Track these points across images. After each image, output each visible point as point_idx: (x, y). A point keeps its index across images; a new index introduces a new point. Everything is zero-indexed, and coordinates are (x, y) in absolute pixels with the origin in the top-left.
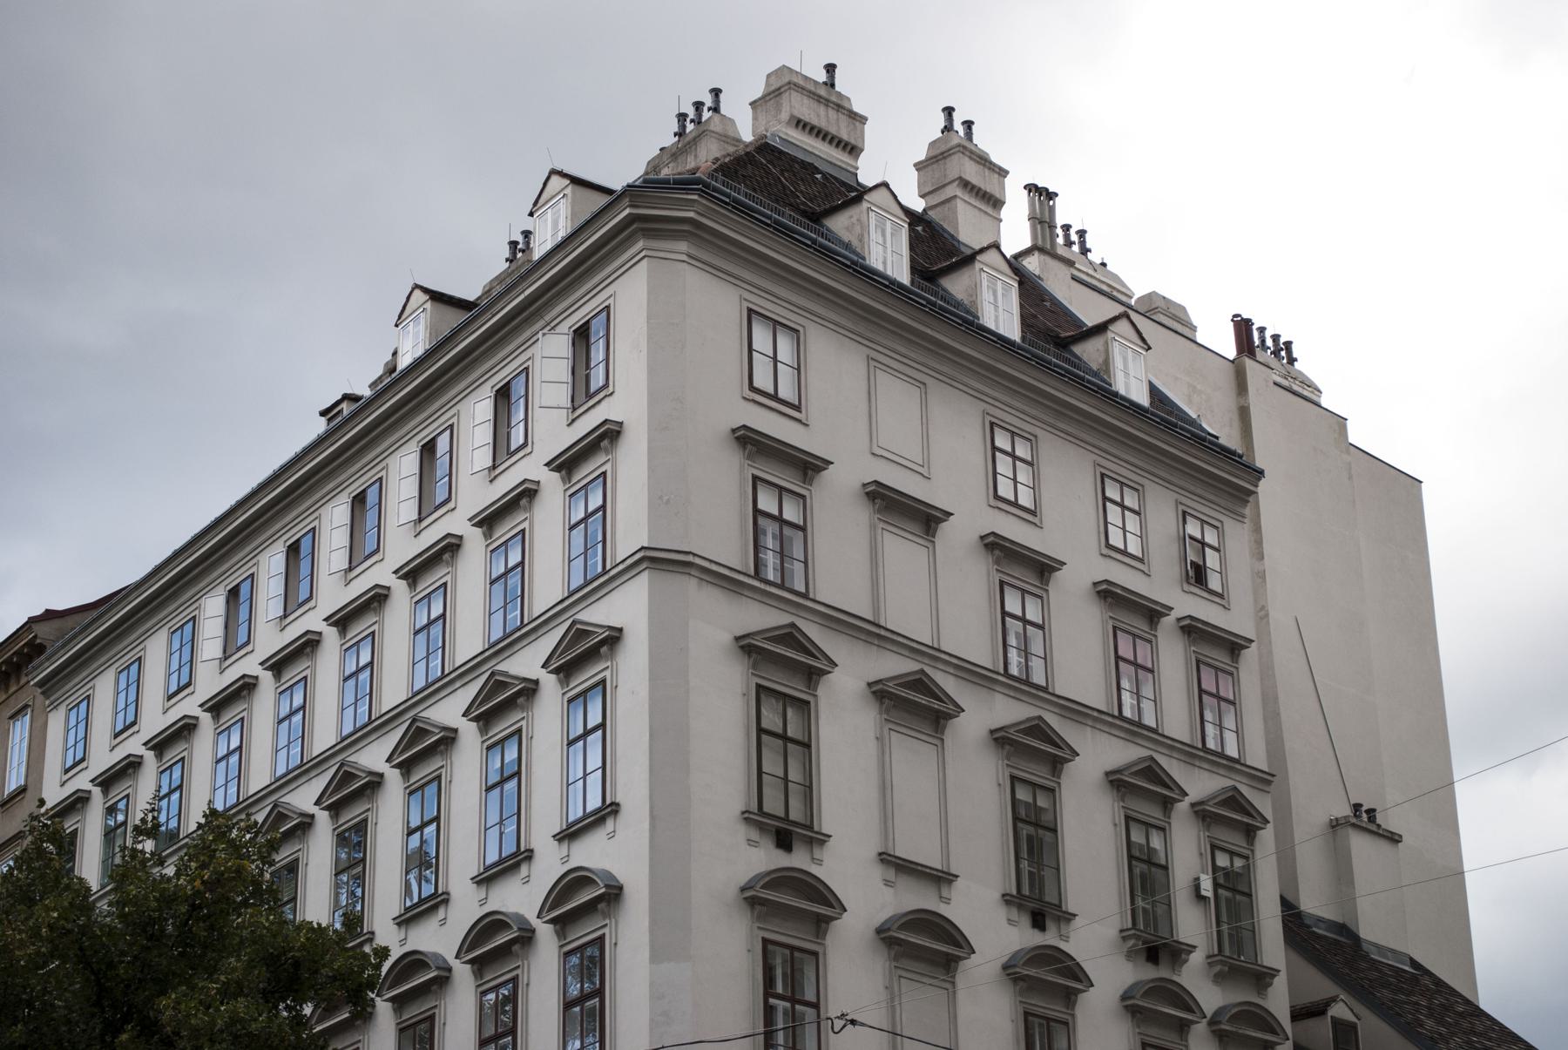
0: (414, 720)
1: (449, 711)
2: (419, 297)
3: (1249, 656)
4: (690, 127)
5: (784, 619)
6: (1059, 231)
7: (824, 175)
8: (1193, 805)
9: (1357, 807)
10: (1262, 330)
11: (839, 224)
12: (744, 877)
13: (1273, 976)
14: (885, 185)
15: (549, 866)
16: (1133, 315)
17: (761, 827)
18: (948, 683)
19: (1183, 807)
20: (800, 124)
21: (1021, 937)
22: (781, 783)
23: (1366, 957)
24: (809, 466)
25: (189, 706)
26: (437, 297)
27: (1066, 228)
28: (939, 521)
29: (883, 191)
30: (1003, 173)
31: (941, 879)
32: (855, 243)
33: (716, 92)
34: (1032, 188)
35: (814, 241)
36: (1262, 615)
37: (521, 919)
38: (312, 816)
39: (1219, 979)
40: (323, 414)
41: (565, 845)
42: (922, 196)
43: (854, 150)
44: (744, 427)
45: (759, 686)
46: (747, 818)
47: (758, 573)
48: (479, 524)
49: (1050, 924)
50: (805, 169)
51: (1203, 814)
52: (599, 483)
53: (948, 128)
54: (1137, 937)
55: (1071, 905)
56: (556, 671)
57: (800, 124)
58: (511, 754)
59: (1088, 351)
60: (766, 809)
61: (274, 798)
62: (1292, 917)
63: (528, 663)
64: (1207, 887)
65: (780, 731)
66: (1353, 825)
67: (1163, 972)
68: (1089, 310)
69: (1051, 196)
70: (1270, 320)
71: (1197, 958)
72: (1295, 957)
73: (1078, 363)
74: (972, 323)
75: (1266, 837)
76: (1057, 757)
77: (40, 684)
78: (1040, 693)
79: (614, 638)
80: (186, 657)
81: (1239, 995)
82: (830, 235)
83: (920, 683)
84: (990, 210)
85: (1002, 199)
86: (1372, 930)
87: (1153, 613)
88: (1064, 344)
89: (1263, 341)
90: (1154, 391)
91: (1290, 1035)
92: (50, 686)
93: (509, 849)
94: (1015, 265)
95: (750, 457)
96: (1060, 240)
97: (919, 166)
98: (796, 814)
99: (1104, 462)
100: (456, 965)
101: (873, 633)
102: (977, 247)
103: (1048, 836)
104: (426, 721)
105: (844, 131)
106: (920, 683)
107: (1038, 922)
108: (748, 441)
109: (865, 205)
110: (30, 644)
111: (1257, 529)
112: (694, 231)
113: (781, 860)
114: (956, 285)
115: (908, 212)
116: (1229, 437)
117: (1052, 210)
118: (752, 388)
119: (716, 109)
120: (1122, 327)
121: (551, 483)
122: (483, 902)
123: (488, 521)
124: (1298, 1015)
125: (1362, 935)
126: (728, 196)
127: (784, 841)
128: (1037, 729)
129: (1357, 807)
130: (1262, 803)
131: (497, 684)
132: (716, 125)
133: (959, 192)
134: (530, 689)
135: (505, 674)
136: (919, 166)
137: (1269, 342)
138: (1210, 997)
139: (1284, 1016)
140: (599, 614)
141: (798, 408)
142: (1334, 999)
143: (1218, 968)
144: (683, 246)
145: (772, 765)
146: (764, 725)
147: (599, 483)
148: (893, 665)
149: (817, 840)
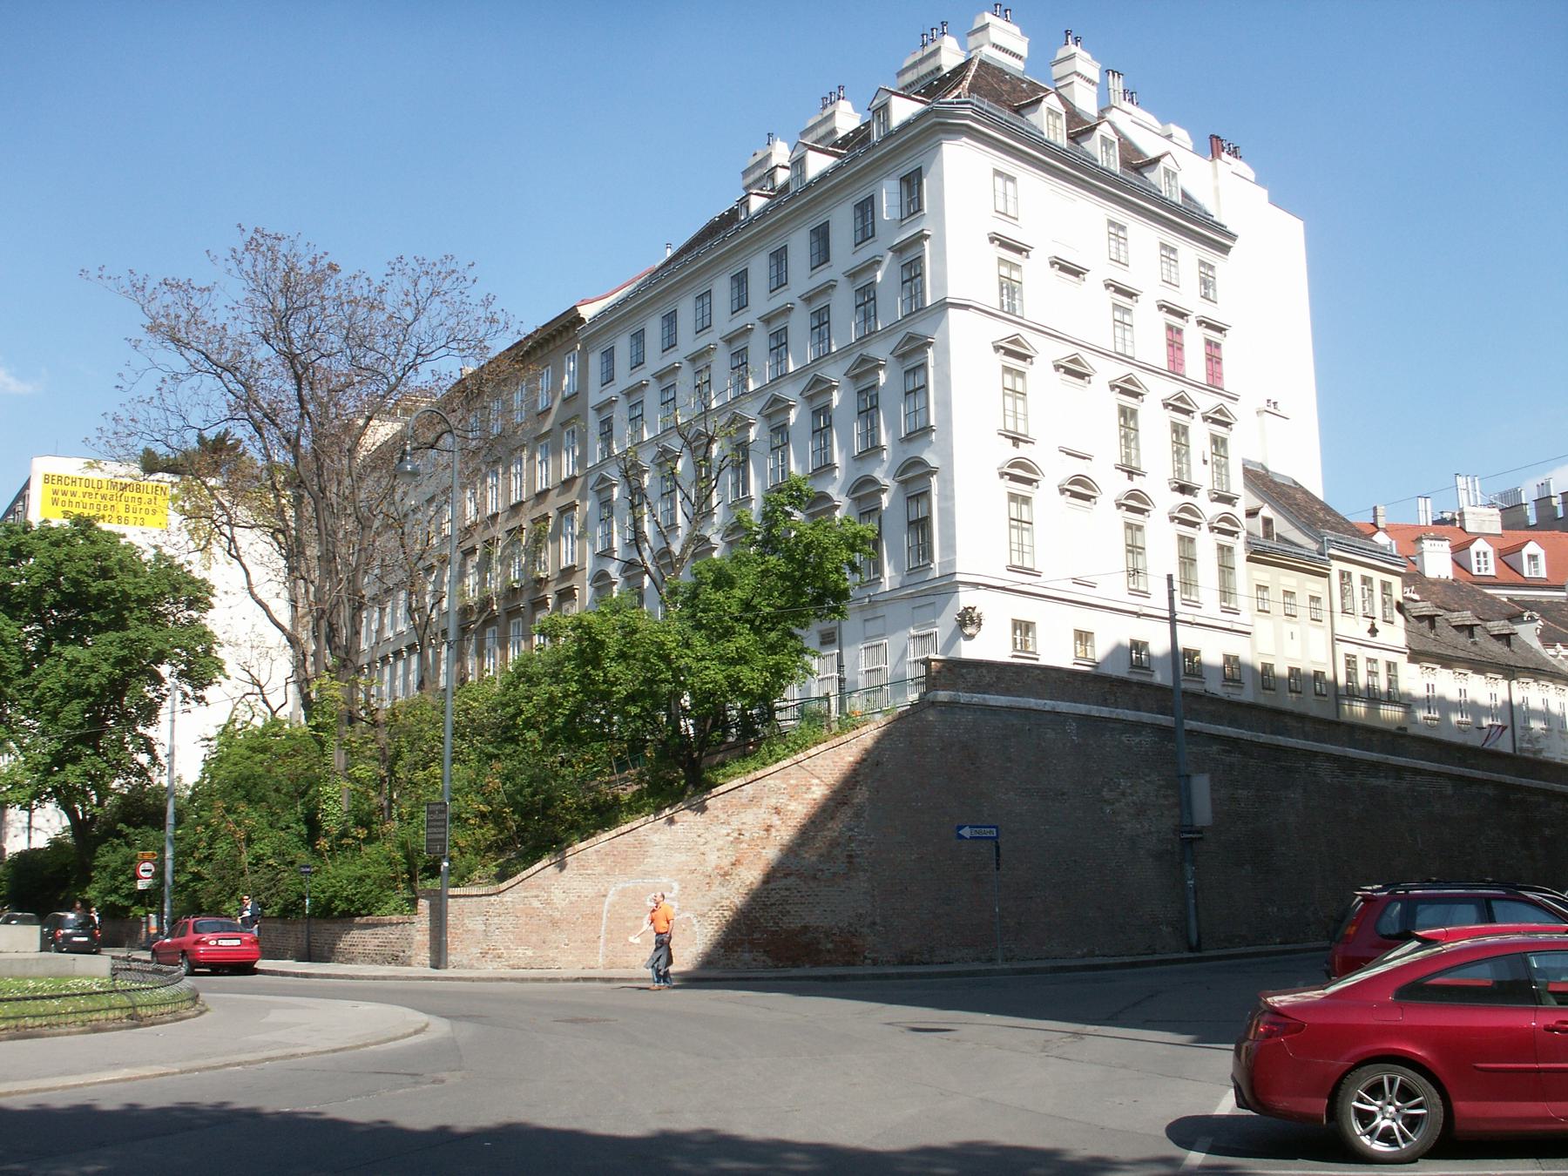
19: (1198, 415)
20: (995, 46)
21: (1123, 484)
41: (906, 443)
57: (995, 46)
67: (1187, 498)
99: (1111, 214)
127: (1016, 441)
148: (1064, 351)
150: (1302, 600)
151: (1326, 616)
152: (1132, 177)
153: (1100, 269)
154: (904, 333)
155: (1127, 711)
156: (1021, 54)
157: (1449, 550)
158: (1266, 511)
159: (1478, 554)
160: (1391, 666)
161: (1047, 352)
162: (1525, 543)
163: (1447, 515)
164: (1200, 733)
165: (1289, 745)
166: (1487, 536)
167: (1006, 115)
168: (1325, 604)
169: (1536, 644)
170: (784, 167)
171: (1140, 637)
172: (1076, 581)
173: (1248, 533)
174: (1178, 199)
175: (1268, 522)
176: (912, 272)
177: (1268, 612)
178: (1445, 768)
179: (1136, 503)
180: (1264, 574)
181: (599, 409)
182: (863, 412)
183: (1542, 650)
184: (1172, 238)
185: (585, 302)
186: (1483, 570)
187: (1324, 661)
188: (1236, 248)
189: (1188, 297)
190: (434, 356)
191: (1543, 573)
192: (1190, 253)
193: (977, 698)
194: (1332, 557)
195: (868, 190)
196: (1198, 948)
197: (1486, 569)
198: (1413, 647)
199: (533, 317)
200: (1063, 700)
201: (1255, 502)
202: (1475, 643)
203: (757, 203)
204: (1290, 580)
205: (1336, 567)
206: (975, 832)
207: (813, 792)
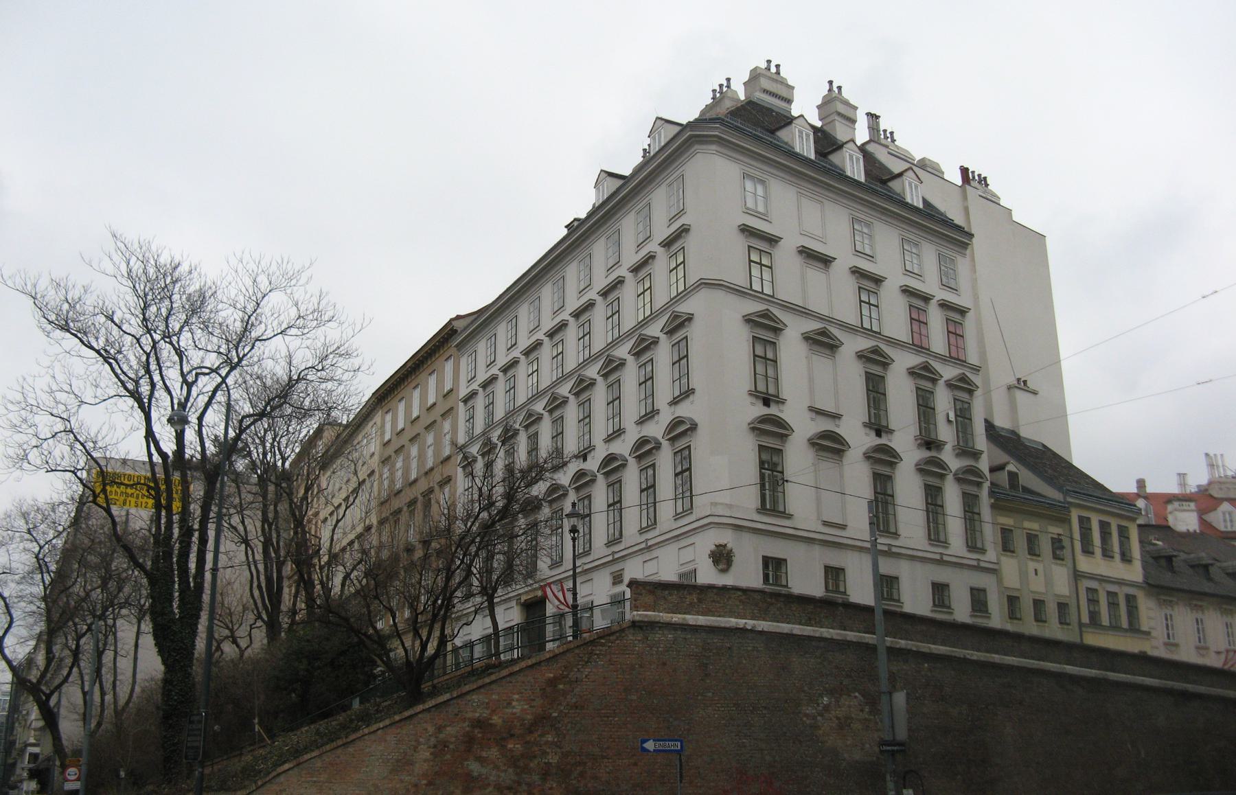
0: (608, 356)
1: (622, 352)
2: (603, 175)
3: (970, 315)
4: (718, 95)
6: (882, 133)
7: (776, 113)
8: (945, 381)
9: (1019, 380)
10: (973, 172)
11: (783, 134)
12: (749, 420)
13: (981, 454)
14: (802, 116)
15: (665, 417)
16: (914, 168)
17: (757, 397)
18: (835, 331)
19: (941, 382)
20: (765, 91)
21: (871, 440)
22: (869, 319)
24: (773, 240)
25: (516, 353)
26: (611, 175)
27: (885, 131)
28: (831, 262)
29: (802, 118)
30: (855, 108)
31: (836, 417)
32: (790, 143)
33: (728, 80)
34: (869, 114)
35: (771, 142)
36: (976, 298)
37: (656, 439)
38: (568, 398)
39: (958, 455)
40: (566, 227)
41: (673, 406)
43: (789, 101)
44: (744, 224)
45: (754, 337)
46: (751, 394)
47: (751, 289)
48: (632, 272)
49: (883, 434)
50: (766, 111)
51: (949, 385)
52: (808, 150)
53: (830, 90)
54: (922, 439)
55: (891, 426)
56: (666, 333)
57: (765, 91)
58: (649, 368)
59: (894, 185)
60: (758, 389)
61: (552, 391)
62: (989, 426)
63: (654, 330)
64: (952, 417)
65: (763, 356)
66: (1016, 387)
67: (933, 453)
68: (896, 166)
69: (877, 117)
70: (975, 167)
71: (948, 448)
72: (993, 447)
73: (890, 190)
74: (842, 175)
75: (978, 393)
76: (885, 364)
77: (456, 346)
79: (690, 318)
80: (514, 333)
81: (966, 462)
82: (779, 139)
83: (823, 333)
84: (850, 124)
85: (854, 118)
86: (1026, 432)
87: (926, 299)
88: (884, 182)
89: (974, 177)
90: (925, 201)
91: (989, 478)
92: (460, 346)
93: (685, 389)
94: (862, 149)
95: (746, 237)
96: (882, 137)
97: (819, 107)
98: (772, 391)
99: (903, 234)
100: (662, 440)
101: (803, 312)
102: (845, 141)
103: (882, 397)
104: (613, 356)
105: (784, 93)
106: (823, 333)
107: (879, 434)
108: (746, 230)
109: (793, 125)
110: (451, 330)
111: (973, 260)
112: (720, 141)
113: (765, 411)
114: (835, 158)
115: (813, 127)
116: (959, 220)
117: (878, 124)
119: (728, 87)
120: (910, 173)
121: (629, 277)
122: (607, 450)
123: (636, 270)
124: (992, 470)
125: (1021, 435)
126: (732, 124)
127: (767, 402)
128: (876, 351)
129: (1019, 380)
130: (976, 379)
131: (642, 339)
132: (729, 94)
133: (836, 118)
134: (655, 341)
135: (645, 335)
136: (819, 107)
137: (977, 178)
138: (954, 463)
139: (986, 472)
140: (684, 308)
142: (1008, 463)
143: (957, 451)
144: (714, 147)
146: (757, 353)
147: (808, 150)
148: (815, 325)
149: (781, 401)
155: (831, 630)
159: (1224, 513)
160: (1130, 599)
164: (909, 651)
165: (1006, 662)
171: (723, 542)
173: (992, 483)
178: (1170, 684)
187: (1067, 593)
189: (930, 285)
193: (677, 618)
200: (764, 620)
205: (1075, 515)
206: (660, 745)
207: (514, 707)
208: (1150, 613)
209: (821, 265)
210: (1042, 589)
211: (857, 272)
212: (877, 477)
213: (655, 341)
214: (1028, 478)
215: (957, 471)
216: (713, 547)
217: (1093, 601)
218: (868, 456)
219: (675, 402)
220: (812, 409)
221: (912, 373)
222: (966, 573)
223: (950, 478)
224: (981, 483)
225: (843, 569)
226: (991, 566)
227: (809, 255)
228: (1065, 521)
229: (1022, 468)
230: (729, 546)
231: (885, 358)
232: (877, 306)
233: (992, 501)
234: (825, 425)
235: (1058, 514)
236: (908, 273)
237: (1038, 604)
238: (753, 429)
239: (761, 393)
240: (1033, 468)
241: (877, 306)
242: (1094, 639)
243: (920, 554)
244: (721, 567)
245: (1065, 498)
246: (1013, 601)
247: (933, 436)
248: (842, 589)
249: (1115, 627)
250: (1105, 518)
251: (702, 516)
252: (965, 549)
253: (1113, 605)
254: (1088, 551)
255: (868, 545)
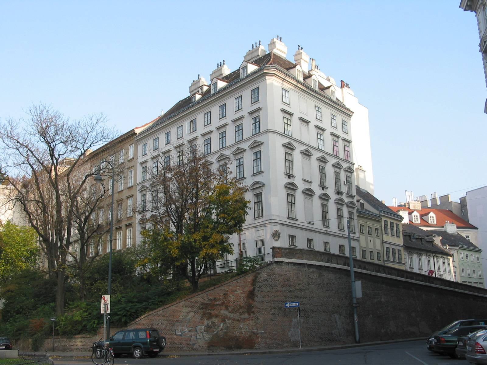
5: (289, 141)
12: (284, 184)
19: (342, 169)
23: (361, 191)
24: (291, 114)
31: (310, 182)
39: (347, 197)
42: (295, 61)
45: (285, 152)
47: (285, 134)
55: (295, 175)
67: (340, 196)
71: (344, 194)
78: (290, 138)
83: (307, 151)
87: (338, 137)
99: (316, 104)
108: (283, 111)
118: (283, 102)
128: (323, 157)
134: (244, 150)
138: (347, 200)
141: (289, 105)
142: (360, 199)
145: (287, 165)
148: (304, 148)
150: (373, 230)
151: (380, 236)
152: (321, 92)
153: (314, 122)
154: (253, 140)
156: (285, 52)
157: (408, 215)
158: (361, 201)
159: (415, 216)
161: (299, 148)
162: (429, 213)
163: (403, 204)
166: (417, 211)
167: (285, 71)
168: (380, 231)
169: (440, 244)
170: (206, 85)
172: (308, 223)
174: (336, 100)
175: (362, 204)
176: (256, 121)
177: (364, 233)
179: (325, 198)
180: (362, 222)
181: (142, 164)
182: (238, 166)
183: (442, 247)
184: (335, 112)
185: (137, 128)
186: (416, 221)
187: (380, 249)
188: (354, 115)
189: (339, 132)
190: (97, 144)
191: (435, 223)
192: (339, 117)
194: (381, 215)
195: (240, 94)
196: (359, 342)
197: (417, 221)
198: (405, 245)
199: (124, 130)
201: (359, 198)
202: (422, 244)
203: (198, 97)
204: (369, 223)
208: (405, 256)
209: (305, 124)
210: (373, 248)
211: (317, 127)
212: (323, 205)
213: (244, 150)
214: (367, 206)
215: (347, 203)
216: (273, 232)
217: (388, 252)
218: (320, 198)
219: (254, 175)
220: (303, 180)
221: (334, 166)
222: (338, 239)
223: (345, 205)
224: (296, 190)
225: (329, 243)
226: (356, 238)
227: (302, 120)
228: (379, 221)
229: (365, 202)
230: (279, 231)
231: (292, 146)
232: (291, 125)
233: (358, 214)
234: (307, 186)
235: (377, 219)
236: (284, 103)
237: (371, 252)
238: (286, 187)
239: (288, 173)
240: (370, 203)
241: (291, 125)
242: (387, 264)
243: (336, 234)
244: (276, 239)
245: (380, 213)
246: (364, 251)
247: (340, 190)
248: (295, 245)
249: (394, 262)
250: (392, 221)
251: (267, 219)
252: (337, 229)
253: (394, 253)
254: (387, 234)
255: (347, 237)
